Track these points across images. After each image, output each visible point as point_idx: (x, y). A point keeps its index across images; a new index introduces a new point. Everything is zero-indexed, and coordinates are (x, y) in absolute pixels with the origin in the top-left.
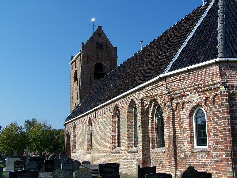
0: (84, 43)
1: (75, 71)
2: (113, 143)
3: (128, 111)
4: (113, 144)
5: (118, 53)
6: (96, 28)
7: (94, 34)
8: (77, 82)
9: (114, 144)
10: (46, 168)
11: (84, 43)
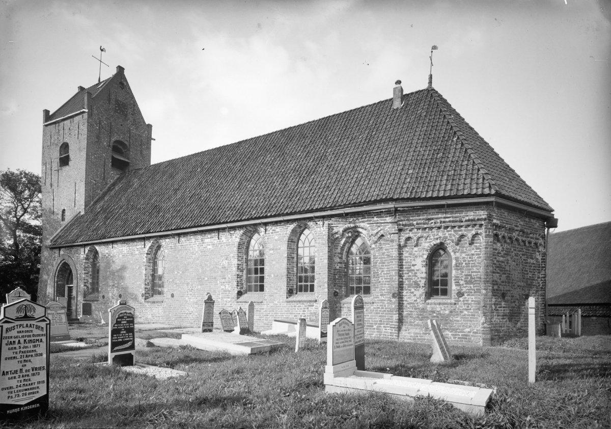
2: (239, 287)
6: (109, 73)
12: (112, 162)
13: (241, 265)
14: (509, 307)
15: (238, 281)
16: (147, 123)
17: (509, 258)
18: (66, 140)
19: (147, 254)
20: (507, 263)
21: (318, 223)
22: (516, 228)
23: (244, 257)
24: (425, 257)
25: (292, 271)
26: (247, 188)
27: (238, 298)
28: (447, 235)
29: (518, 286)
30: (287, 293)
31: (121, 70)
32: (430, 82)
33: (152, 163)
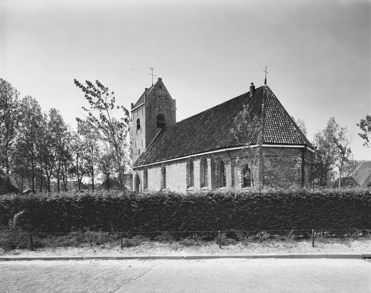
6: (155, 81)
8: (140, 130)
12: (157, 125)
16: (173, 99)
17: (276, 168)
18: (139, 117)
24: (139, 171)
26: (275, 124)
27: (187, 189)
29: (283, 180)
31: (160, 79)
32: (265, 83)
33: (179, 119)
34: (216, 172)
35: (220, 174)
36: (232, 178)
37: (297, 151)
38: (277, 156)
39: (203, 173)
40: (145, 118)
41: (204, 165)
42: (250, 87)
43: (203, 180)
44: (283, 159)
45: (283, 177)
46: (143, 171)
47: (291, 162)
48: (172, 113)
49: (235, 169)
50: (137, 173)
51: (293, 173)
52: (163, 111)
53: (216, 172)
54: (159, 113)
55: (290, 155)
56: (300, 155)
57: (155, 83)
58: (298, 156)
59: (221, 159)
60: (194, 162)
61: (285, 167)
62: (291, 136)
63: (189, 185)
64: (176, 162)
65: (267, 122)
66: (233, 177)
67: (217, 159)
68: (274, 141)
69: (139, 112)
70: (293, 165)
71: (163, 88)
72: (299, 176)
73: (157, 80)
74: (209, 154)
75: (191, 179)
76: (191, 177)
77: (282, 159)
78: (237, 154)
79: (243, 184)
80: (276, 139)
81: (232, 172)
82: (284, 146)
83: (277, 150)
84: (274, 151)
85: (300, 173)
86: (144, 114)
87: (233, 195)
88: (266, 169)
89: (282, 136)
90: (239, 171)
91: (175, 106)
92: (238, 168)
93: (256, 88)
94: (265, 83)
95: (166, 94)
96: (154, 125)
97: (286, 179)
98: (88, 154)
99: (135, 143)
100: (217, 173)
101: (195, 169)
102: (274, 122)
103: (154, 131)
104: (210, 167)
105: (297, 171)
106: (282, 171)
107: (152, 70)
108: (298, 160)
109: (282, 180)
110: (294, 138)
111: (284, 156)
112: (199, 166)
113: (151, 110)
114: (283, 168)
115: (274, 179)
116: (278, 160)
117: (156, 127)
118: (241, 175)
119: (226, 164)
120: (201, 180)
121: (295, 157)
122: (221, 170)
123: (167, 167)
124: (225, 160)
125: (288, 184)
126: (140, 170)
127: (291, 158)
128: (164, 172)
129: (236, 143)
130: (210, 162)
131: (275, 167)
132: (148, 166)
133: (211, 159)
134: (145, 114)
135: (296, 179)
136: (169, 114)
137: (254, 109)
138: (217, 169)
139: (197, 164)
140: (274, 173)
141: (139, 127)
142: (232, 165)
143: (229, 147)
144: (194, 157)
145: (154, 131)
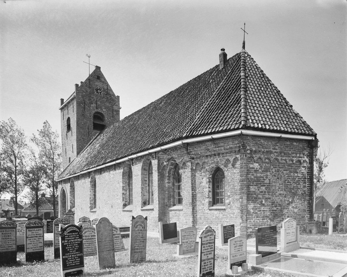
0: (63, 99)
1: (67, 118)
2: (124, 201)
3: (142, 168)
4: (123, 202)
5: (122, 104)
6: (93, 69)
7: (91, 76)
8: (71, 132)
9: (125, 202)
10: (48, 230)
11: (63, 99)
13: (125, 187)
14: (270, 211)
15: (123, 197)
17: (268, 173)
18: (70, 116)
19: (90, 182)
20: (267, 177)
21: (273, 142)
22: (274, 151)
23: (127, 181)
24: (65, 185)
25: (146, 190)
27: (123, 208)
28: (218, 160)
29: (280, 194)
30: (142, 204)
31: (98, 68)
32: (244, 47)
34: (167, 181)
35: (173, 185)
36: (192, 190)
37: (301, 146)
38: (271, 152)
39: (146, 184)
40: (76, 115)
41: (147, 170)
42: (220, 55)
43: (147, 194)
44: (279, 158)
45: (279, 188)
46: (69, 185)
47: (292, 164)
48: (115, 113)
49: (197, 175)
50: (63, 188)
51: (295, 183)
52: (101, 109)
53: (167, 181)
54: (96, 110)
55: (290, 153)
56: (306, 153)
57: (91, 71)
58: (304, 154)
59: (175, 161)
60: (133, 167)
61: (282, 172)
62: (291, 120)
63: (127, 203)
64: (109, 168)
65: (251, 98)
66: (193, 188)
67: (169, 160)
68: (265, 126)
69: (69, 109)
70: (295, 169)
71: (102, 79)
72: (304, 187)
73: (94, 68)
74: (155, 152)
75: (129, 194)
76: (129, 191)
77: (278, 158)
78: (202, 150)
79: (211, 200)
80: (269, 123)
81: (192, 181)
82: (284, 136)
83: (270, 143)
84: (266, 143)
85: (305, 183)
86: (75, 110)
87: (309, 207)
88: (253, 175)
89: (278, 120)
90: (205, 179)
91: (119, 104)
92: (203, 174)
93: (228, 58)
94: (244, 47)
95: (106, 88)
96: (89, 126)
97: (285, 193)
98: (10, 164)
99: (65, 150)
100: (168, 183)
101: (134, 177)
102: (261, 99)
103: (89, 133)
104: (157, 173)
105: (301, 179)
106: (278, 178)
107: (89, 57)
108: (304, 161)
109: (277, 194)
110: (296, 124)
111: (281, 153)
112: (140, 173)
113: (84, 105)
114: (280, 173)
115: (265, 192)
116: (272, 159)
117: (92, 129)
118: (207, 186)
119: (182, 168)
120: (143, 195)
121: (298, 155)
122: (174, 178)
123: (97, 177)
124: (181, 160)
125: (288, 201)
126: (67, 183)
127: (293, 157)
128: (94, 185)
129: (200, 130)
130: (157, 166)
131: (267, 171)
132: (75, 176)
133: (159, 161)
134: (76, 110)
135: (300, 192)
136: (110, 114)
137: (227, 81)
138: (168, 176)
139: (137, 169)
140: (266, 182)
141: (69, 128)
142: (192, 169)
143: (187, 137)
144: (132, 159)
145: (89, 133)
